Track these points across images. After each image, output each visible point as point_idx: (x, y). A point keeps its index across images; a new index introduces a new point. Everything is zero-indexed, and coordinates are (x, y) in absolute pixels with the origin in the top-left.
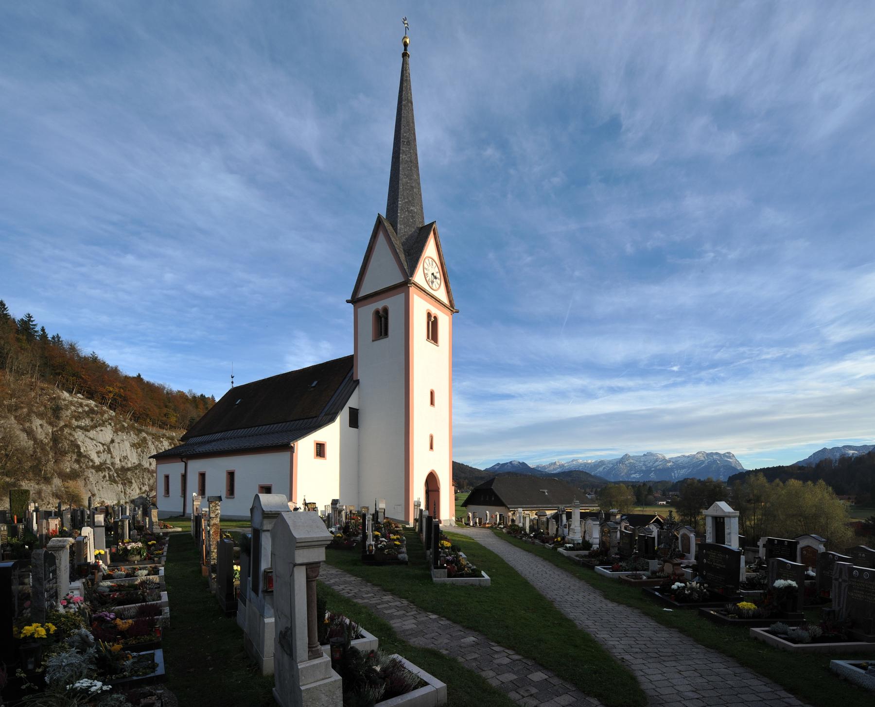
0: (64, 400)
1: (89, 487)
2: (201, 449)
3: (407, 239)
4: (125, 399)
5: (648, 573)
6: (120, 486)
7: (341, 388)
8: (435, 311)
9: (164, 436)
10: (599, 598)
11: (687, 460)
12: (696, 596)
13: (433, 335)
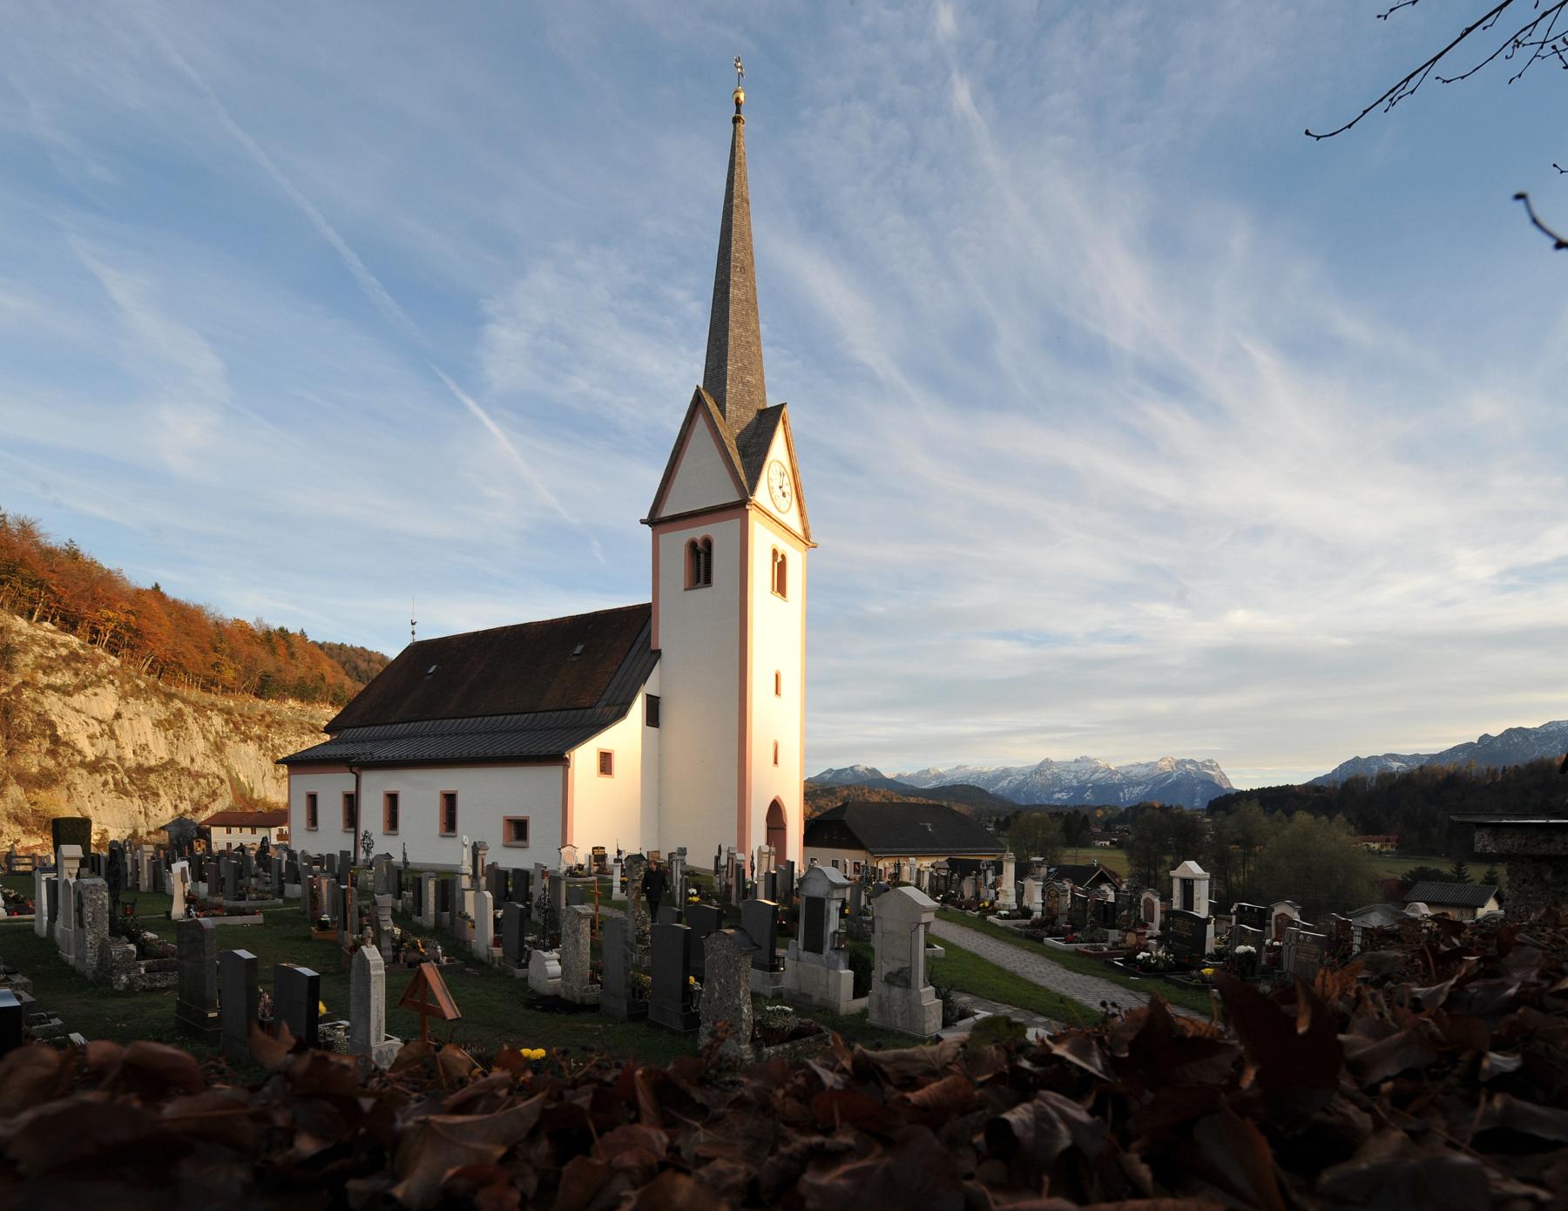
0: (19, 633)
1: (77, 802)
2: (383, 752)
4: (137, 633)
5: (1109, 944)
6: (137, 801)
7: (628, 661)
9: (213, 706)
10: (1062, 970)
11: (1145, 771)
12: (1161, 965)
13: (781, 587)
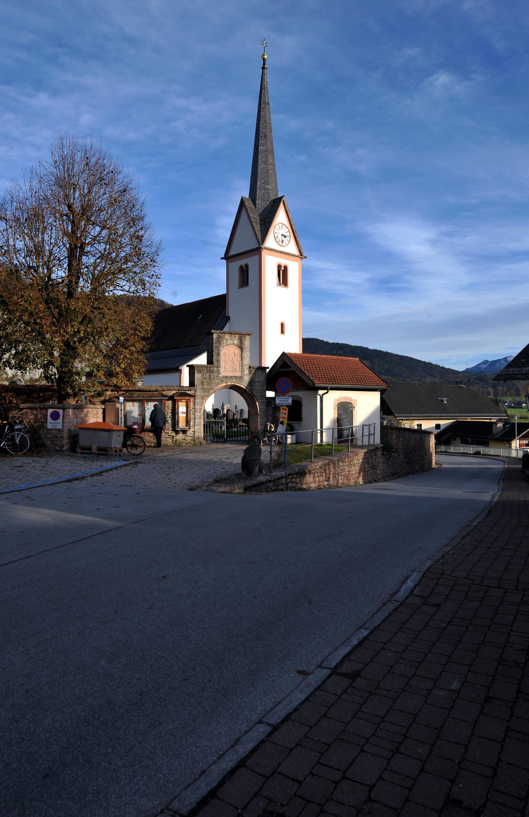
3: (263, 211)
8: (284, 262)
